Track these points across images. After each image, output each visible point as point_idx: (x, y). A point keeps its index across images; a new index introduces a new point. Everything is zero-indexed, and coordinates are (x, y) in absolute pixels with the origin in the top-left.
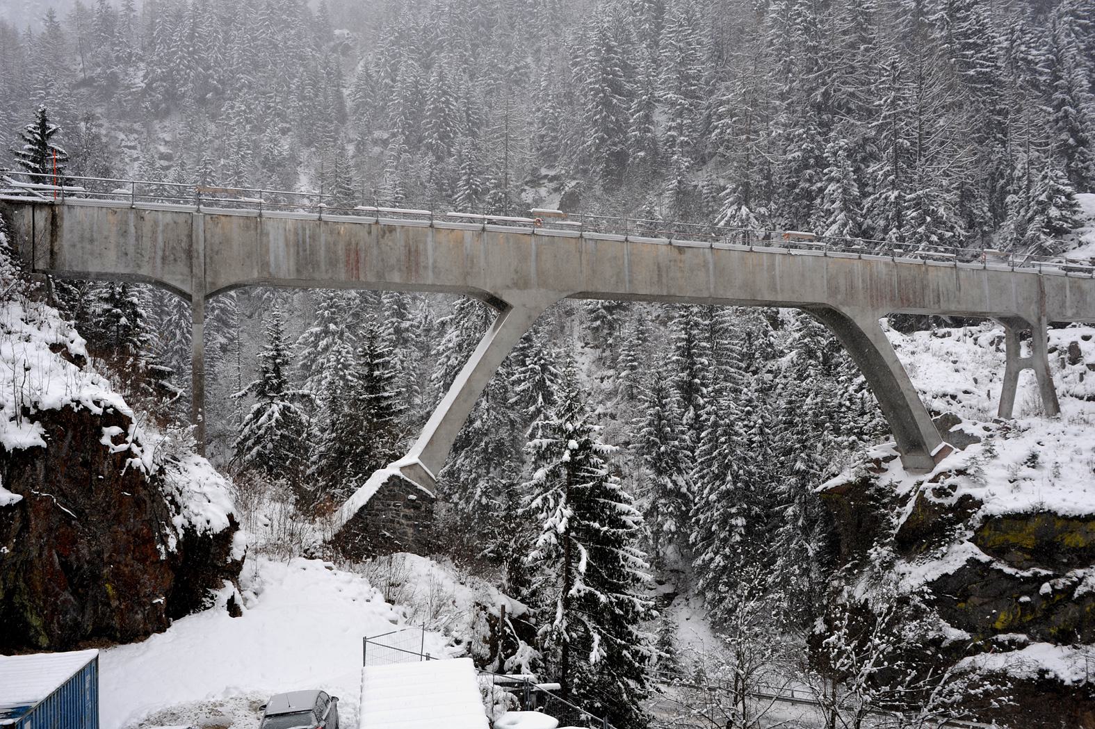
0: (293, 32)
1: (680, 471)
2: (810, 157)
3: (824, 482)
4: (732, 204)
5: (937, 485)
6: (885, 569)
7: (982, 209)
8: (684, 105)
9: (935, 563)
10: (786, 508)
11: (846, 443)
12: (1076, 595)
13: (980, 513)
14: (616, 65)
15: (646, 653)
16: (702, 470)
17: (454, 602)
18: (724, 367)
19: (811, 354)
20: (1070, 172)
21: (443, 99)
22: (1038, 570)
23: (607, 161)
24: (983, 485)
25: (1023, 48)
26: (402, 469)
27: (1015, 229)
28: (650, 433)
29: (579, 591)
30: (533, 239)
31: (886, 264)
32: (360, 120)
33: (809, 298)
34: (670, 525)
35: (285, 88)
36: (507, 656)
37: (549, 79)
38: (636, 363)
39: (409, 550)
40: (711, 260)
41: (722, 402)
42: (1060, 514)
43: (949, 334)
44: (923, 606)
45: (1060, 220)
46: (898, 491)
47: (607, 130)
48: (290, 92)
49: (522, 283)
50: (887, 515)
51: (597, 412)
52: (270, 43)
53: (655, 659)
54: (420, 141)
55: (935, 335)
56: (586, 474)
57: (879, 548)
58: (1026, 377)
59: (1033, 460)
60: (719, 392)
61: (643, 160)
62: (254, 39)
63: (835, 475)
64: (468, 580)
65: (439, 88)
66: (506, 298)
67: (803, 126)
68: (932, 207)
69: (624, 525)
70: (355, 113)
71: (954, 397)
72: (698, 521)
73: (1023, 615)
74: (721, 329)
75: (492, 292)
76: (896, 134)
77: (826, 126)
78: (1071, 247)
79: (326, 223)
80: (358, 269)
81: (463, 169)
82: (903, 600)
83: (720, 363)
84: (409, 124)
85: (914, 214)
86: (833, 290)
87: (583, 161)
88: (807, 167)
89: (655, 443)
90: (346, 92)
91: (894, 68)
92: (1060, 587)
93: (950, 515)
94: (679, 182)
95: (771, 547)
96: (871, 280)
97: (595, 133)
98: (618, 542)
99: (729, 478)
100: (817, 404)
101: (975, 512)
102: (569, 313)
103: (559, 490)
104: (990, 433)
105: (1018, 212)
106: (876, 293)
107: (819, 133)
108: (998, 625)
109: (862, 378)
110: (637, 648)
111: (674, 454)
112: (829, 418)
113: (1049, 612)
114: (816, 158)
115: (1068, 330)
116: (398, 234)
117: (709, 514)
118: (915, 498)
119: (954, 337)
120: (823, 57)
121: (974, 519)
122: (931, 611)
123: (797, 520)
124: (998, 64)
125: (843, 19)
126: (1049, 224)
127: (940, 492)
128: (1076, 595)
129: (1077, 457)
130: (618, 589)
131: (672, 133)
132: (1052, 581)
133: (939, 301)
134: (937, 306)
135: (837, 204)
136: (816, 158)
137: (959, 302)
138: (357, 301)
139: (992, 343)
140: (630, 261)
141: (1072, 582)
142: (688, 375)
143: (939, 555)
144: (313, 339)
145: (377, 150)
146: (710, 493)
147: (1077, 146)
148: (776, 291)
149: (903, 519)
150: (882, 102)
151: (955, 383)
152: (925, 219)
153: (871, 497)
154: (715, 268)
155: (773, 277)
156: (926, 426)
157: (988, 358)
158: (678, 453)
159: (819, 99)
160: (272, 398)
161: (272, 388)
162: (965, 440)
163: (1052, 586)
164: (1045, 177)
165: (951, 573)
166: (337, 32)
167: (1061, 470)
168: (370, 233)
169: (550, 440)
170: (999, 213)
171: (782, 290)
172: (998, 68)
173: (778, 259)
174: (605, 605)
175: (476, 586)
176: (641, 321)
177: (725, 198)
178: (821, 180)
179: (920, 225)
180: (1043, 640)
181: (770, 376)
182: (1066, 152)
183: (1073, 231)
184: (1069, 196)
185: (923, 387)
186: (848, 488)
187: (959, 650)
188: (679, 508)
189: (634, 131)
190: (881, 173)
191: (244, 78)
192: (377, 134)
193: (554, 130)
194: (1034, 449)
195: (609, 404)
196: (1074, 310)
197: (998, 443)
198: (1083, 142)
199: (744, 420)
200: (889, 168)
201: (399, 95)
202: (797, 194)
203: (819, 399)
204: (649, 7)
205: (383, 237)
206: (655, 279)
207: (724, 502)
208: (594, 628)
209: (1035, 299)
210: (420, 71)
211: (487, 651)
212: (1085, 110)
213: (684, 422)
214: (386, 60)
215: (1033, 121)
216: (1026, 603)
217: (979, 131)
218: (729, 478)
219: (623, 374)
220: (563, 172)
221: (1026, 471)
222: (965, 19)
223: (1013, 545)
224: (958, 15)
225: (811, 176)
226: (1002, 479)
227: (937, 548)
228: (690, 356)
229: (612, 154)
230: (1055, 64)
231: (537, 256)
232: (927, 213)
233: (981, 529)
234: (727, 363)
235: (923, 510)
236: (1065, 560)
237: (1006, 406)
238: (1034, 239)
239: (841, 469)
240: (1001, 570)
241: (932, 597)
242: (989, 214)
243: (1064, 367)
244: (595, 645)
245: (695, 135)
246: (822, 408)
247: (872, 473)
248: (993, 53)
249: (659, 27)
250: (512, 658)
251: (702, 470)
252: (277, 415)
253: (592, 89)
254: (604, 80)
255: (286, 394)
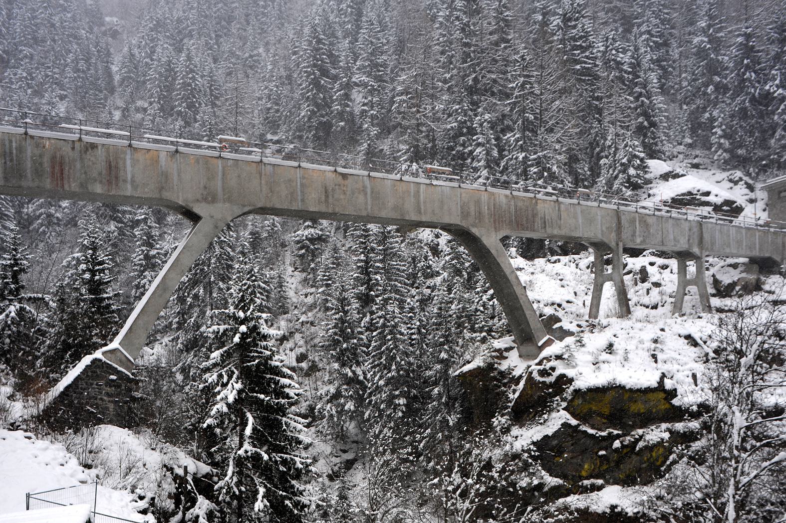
0: (69, 15)
1: (358, 364)
2: (463, 127)
3: (461, 368)
4: (406, 161)
5: (541, 367)
6: (503, 433)
7: (584, 168)
8: (373, 86)
9: (539, 427)
10: (433, 389)
11: (479, 338)
12: (637, 449)
13: (572, 388)
14: (324, 54)
15: (307, 502)
16: (374, 361)
17: (144, 465)
18: (393, 283)
19: (458, 272)
20: (643, 143)
21: (190, 76)
22: (611, 430)
23: (317, 129)
24: (574, 367)
25: (614, 52)
26: (104, 353)
27: (606, 184)
28: (335, 334)
29: (246, 452)
30: (220, 161)
31: (506, 196)
32: (125, 91)
33: (447, 220)
34: (350, 406)
35: (62, 61)
36: (188, 509)
37: (274, 64)
38: (330, 282)
39: (111, 422)
40: (368, 186)
41: (389, 308)
42: (627, 388)
43: (559, 261)
44: (530, 461)
45: (635, 177)
46: (514, 373)
47: (317, 105)
48: (67, 65)
49: (210, 198)
50: (506, 392)
51: (300, 321)
52: (49, 22)
53: (313, 507)
54: (172, 109)
55: (549, 261)
56: (256, 354)
57: (499, 418)
58: (609, 289)
59: (610, 348)
60: (386, 301)
61: (343, 128)
62: (34, 18)
63: (469, 362)
64: (158, 446)
65: (187, 67)
66: (197, 209)
67: (459, 103)
68: (548, 165)
69: (287, 396)
70: (121, 85)
71: (559, 305)
72: (371, 401)
73: (601, 464)
74: (391, 253)
75: (184, 205)
76: (523, 111)
77: (475, 104)
78: (643, 198)
79: (32, 137)
80: (62, 179)
81: (205, 131)
82: (516, 456)
83: (390, 279)
84: (164, 95)
85: (536, 170)
86: (465, 215)
87: (299, 129)
88: (462, 135)
89: (339, 341)
90: (114, 68)
91: (523, 59)
92: (626, 443)
93: (551, 390)
94: (369, 145)
95: (422, 419)
96: (494, 208)
97: (308, 106)
98: (282, 410)
99: (394, 367)
100: (459, 309)
101: (568, 388)
102: (283, 245)
103: (233, 368)
104: (582, 329)
105: (608, 171)
106: (498, 218)
107: (471, 110)
108: (584, 474)
109: (491, 292)
110: (298, 498)
111: (353, 351)
112: (467, 319)
113: (618, 463)
114: (468, 128)
115: (640, 258)
116: (100, 151)
117: (379, 396)
118: (525, 378)
119: (562, 262)
120: (474, 52)
121: (567, 393)
122: (536, 464)
123: (441, 398)
124: (597, 63)
125: (489, 23)
126: (628, 181)
127: (543, 373)
128: (637, 449)
129: (640, 346)
130: (281, 450)
131: (365, 108)
132: (621, 439)
133: (545, 227)
134: (543, 231)
135: (482, 163)
136: (468, 128)
137: (560, 227)
138: (116, 234)
139: (588, 267)
140: (302, 185)
141: (635, 439)
142: (366, 289)
143: (542, 421)
144: (74, 262)
145: (139, 116)
146: (379, 380)
147: (650, 127)
148: (420, 213)
149: (517, 394)
150: (514, 85)
151: (560, 296)
152: (543, 174)
153: (495, 378)
154: (372, 192)
155: (418, 203)
156: (535, 325)
157: (585, 277)
158: (356, 349)
159: (470, 82)
160: (11, 300)
161: (11, 292)
162: (564, 334)
163: (621, 442)
164: (626, 146)
165: (550, 434)
166: (108, 19)
167: (629, 355)
168: (73, 148)
169: (226, 326)
170: (595, 171)
171: (425, 213)
172: (597, 66)
173: (422, 187)
174: (266, 462)
175: (165, 451)
176: (336, 250)
177: (400, 157)
178: (471, 145)
179: (540, 179)
180: (616, 483)
181: (429, 291)
182: (641, 131)
183: (645, 186)
184: (642, 160)
185: (538, 298)
186: (478, 371)
187: (557, 493)
188: (358, 392)
189: (336, 105)
190: (513, 139)
191: (27, 51)
192: (139, 103)
193: (277, 104)
194: (611, 340)
195: (310, 314)
196: (641, 239)
197: (587, 337)
198: (653, 124)
199: (407, 324)
200: (518, 136)
201: (155, 71)
202: (454, 155)
203: (460, 306)
204: (351, 12)
205: (86, 152)
206: (323, 198)
207: (390, 387)
208: (261, 483)
209: (615, 229)
210: (173, 53)
211: (173, 506)
212: (655, 101)
213: (362, 325)
214: (146, 43)
215: (618, 104)
216: (603, 456)
217: (583, 110)
218: (394, 367)
219: (321, 290)
220: (284, 137)
221: (605, 356)
222: (575, 27)
223: (595, 412)
224: (569, 24)
225: (464, 142)
226: (587, 362)
227: (540, 416)
228: (368, 274)
229: (321, 123)
230: (636, 65)
231: (223, 175)
232: (544, 169)
233: (572, 400)
234: (396, 280)
235: (531, 388)
236: (631, 423)
237: (594, 310)
238: (619, 191)
239: (474, 357)
240: (586, 432)
241: (537, 454)
242: (588, 173)
243: (636, 284)
244: (260, 497)
245: (383, 111)
246: (463, 312)
247: (496, 360)
248: (593, 54)
249: (359, 27)
250: (192, 510)
251: (374, 361)
252: (13, 314)
253: (306, 72)
254: (315, 65)
255: (22, 297)
